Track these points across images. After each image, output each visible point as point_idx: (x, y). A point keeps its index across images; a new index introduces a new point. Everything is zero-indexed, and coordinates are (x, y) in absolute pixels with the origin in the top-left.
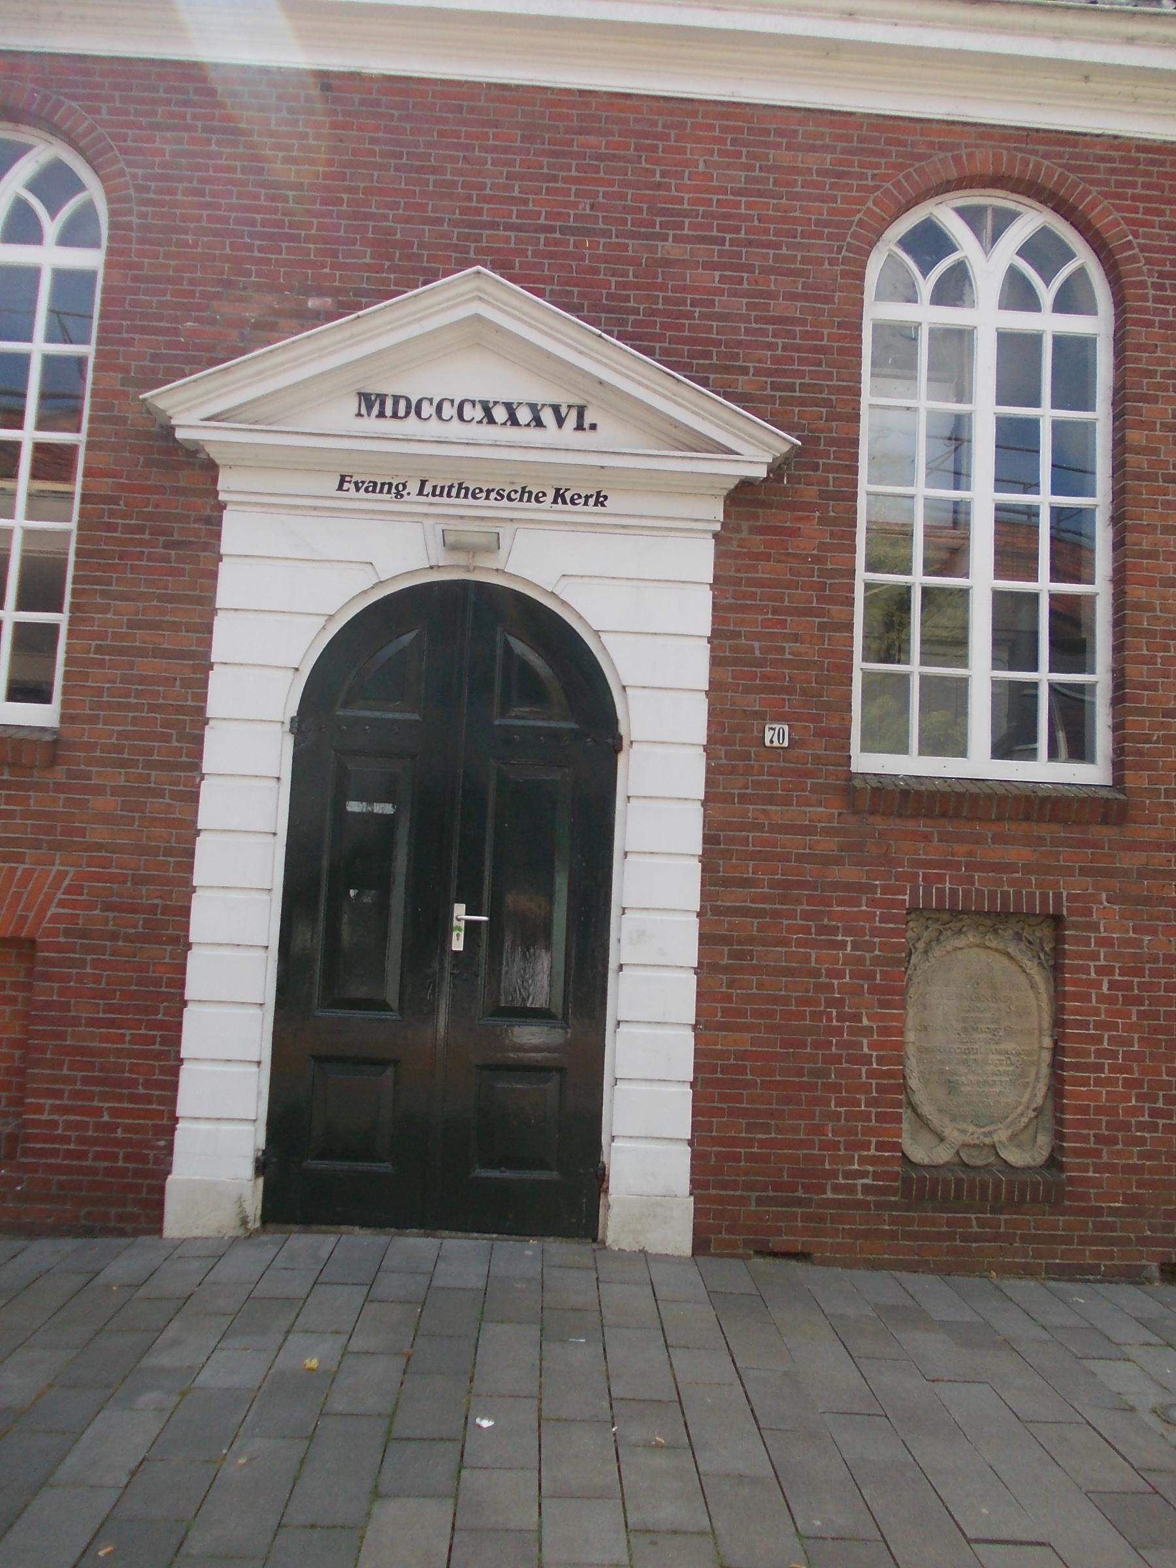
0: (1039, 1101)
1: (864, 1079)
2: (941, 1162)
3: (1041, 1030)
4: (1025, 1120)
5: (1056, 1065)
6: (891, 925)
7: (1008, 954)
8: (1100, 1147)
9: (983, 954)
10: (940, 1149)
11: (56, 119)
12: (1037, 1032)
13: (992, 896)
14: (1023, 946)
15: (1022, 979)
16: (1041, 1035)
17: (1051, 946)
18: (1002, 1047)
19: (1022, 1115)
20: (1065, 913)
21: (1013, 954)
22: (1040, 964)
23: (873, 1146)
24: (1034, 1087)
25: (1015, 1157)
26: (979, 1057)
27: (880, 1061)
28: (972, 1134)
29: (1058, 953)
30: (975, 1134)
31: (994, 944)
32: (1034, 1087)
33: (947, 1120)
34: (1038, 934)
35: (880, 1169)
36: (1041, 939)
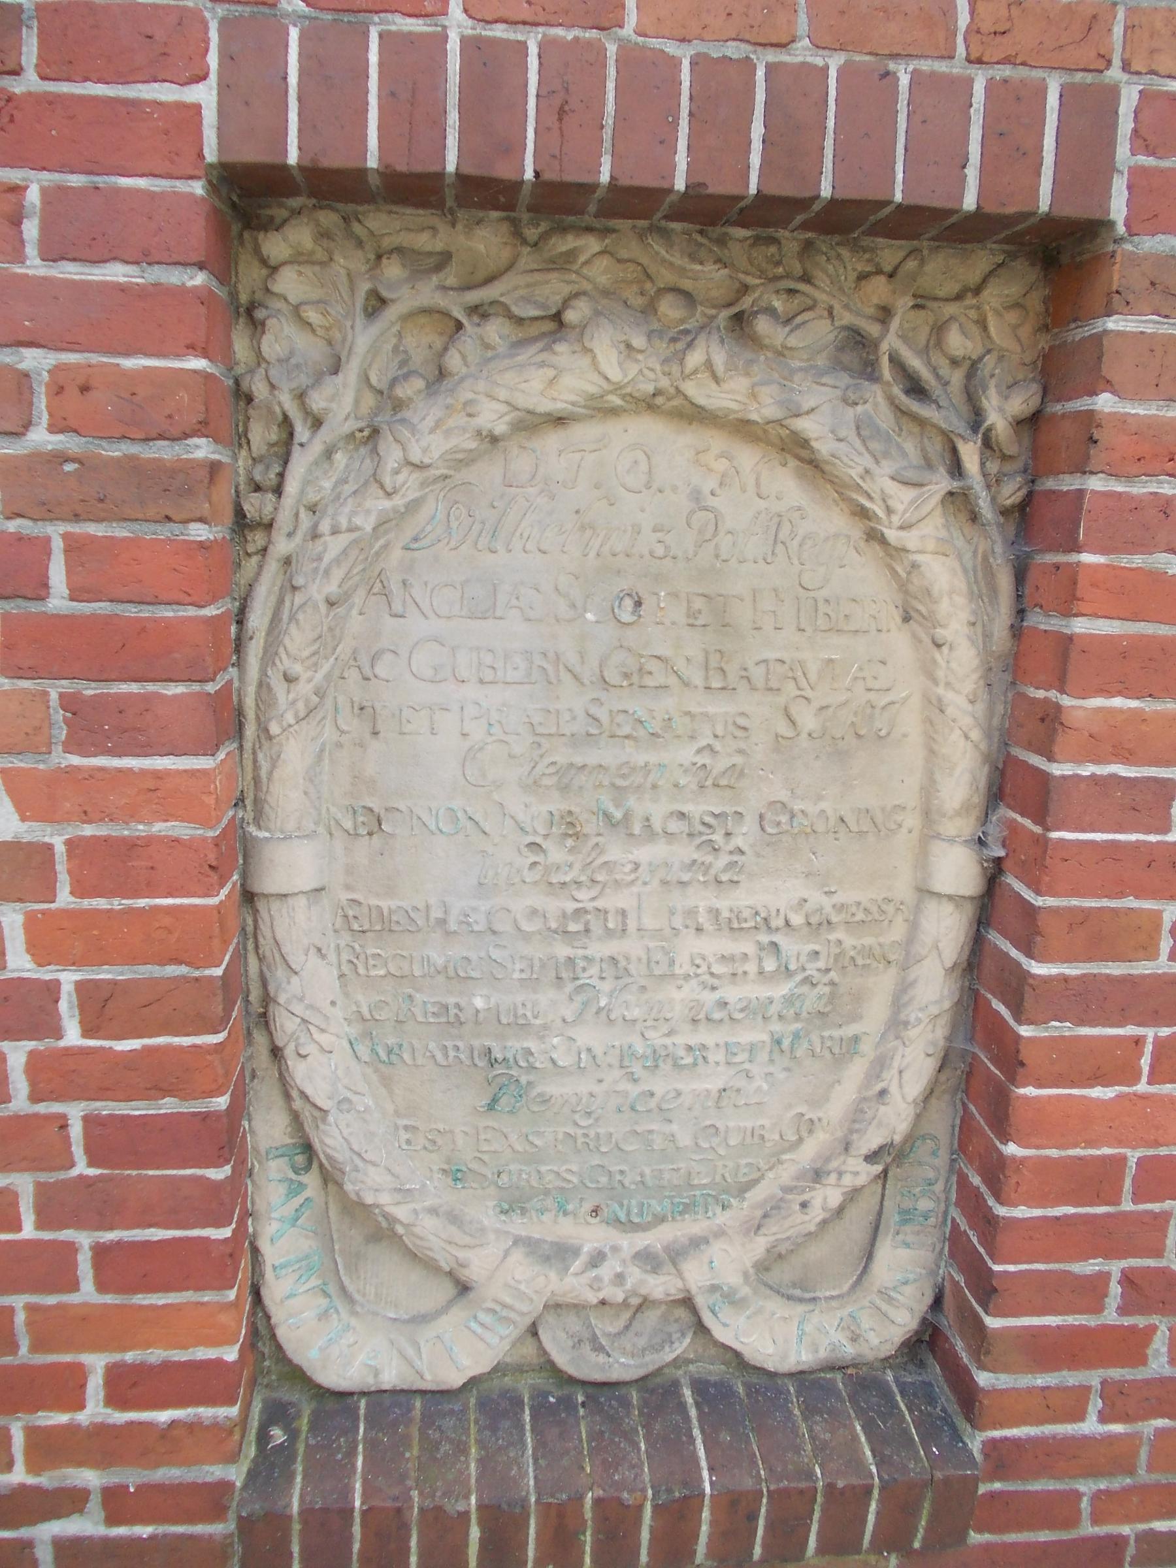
0: (894, 1119)
1: (20, 1101)
2: (456, 1380)
3: (928, 814)
4: (829, 1195)
5: (984, 978)
6: (117, 273)
7: (797, 450)
8: (1141, 1321)
9: (674, 449)
10: (450, 1324)
11: (1083, 707)
12: (912, 820)
13: (721, 90)
14: (876, 402)
15: (862, 577)
16: (929, 835)
17: (1020, 403)
18: (742, 899)
19: (818, 1175)
20: (1118, 209)
21: (824, 447)
22: (959, 502)
23: (95, 1385)
24: (880, 1064)
25: (777, 1338)
26: (632, 947)
27: (99, 1007)
28: (598, 1258)
29: (1048, 440)
30: (611, 1262)
31: (728, 396)
32: (880, 1064)
33: (484, 1213)
34: (957, 342)
35: (132, 1477)
36: (973, 367)
